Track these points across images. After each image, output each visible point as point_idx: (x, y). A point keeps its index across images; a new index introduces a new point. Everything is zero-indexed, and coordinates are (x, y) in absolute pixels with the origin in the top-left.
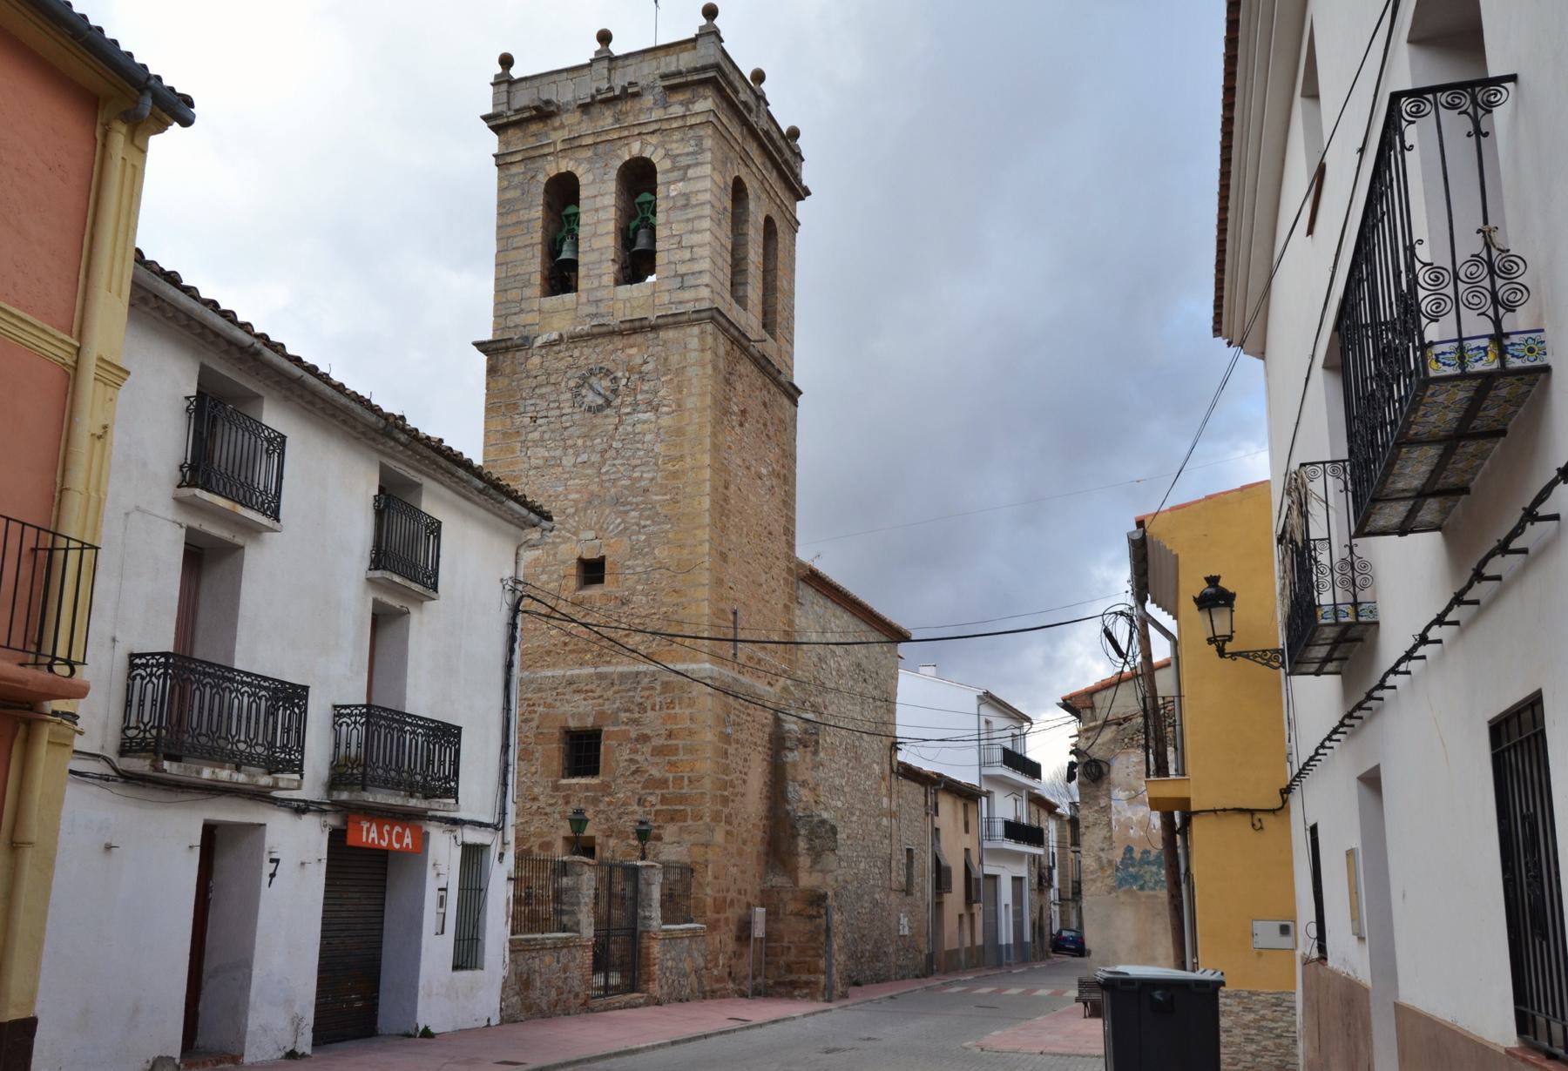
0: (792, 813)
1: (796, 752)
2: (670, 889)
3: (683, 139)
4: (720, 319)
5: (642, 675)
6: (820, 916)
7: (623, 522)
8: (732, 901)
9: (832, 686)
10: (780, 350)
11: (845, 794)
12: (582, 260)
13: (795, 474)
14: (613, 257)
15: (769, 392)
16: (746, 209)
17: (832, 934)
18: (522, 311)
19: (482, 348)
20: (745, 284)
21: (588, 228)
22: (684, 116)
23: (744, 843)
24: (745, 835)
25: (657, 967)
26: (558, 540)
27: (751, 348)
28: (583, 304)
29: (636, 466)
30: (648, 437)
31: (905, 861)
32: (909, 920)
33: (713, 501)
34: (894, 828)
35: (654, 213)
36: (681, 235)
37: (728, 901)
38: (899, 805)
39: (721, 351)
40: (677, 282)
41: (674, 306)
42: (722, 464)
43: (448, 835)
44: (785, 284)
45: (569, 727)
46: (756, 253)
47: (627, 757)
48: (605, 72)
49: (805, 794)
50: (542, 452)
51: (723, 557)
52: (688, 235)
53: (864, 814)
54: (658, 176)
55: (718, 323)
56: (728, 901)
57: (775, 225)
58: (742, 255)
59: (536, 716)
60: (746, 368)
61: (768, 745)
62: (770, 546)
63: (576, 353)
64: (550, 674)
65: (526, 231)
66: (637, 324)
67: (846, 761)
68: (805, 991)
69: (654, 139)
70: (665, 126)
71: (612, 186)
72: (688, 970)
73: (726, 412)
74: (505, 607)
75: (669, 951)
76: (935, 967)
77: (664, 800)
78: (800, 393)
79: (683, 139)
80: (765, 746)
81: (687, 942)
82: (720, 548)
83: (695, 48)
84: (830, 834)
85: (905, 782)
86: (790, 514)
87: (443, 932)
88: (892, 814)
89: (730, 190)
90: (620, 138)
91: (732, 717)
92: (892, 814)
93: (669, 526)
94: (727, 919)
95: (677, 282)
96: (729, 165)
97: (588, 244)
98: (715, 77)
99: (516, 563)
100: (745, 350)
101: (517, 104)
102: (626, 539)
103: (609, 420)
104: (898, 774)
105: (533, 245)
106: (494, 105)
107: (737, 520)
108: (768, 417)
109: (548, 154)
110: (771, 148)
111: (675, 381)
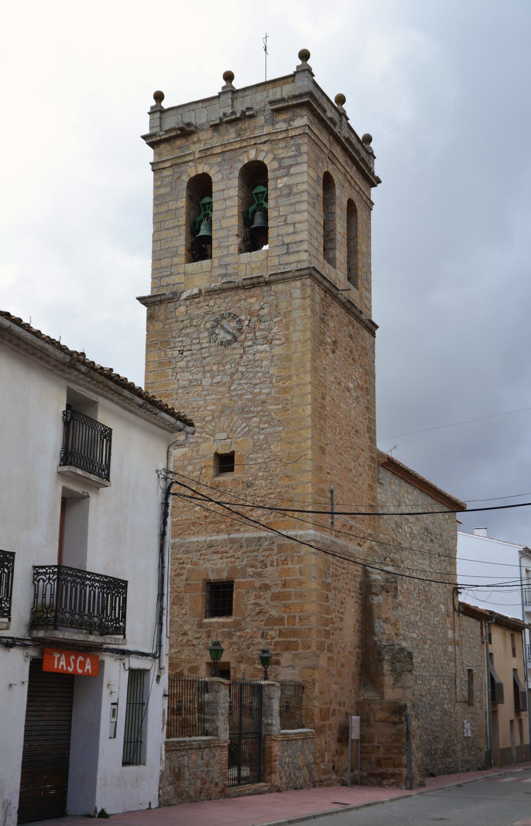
0: (378, 643)
1: (380, 597)
3: (286, 147)
4: (316, 275)
5: (263, 540)
6: (402, 723)
7: (247, 425)
8: (334, 711)
9: (407, 545)
10: (361, 296)
13: (374, 387)
16: (333, 194)
17: (411, 737)
18: (172, 274)
20: (335, 248)
21: (218, 213)
22: (287, 130)
23: (343, 666)
24: (343, 660)
25: (277, 762)
26: (200, 440)
28: (216, 267)
29: (256, 384)
30: (265, 363)
31: (466, 679)
33: (314, 409)
35: (266, 200)
36: (286, 216)
38: (461, 636)
39: (318, 298)
40: (284, 250)
41: (282, 267)
42: (320, 381)
43: (118, 662)
45: (209, 579)
46: (342, 226)
48: (230, 101)
49: (388, 628)
51: (322, 450)
52: (291, 215)
53: (433, 643)
54: (269, 173)
57: (355, 206)
58: (331, 228)
59: (185, 571)
60: (336, 310)
61: (359, 591)
62: (357, 441)
63: (211, 303)
65: (174, 216)
67: (419, 603)
68: (392, 781)
69: (265, 147)
73: (322, 343)
74: (160, 491)
76: (493, 762)
77: (281, 634)
78: (377, 327)
79: (286, 147)
80: (356, 592)
81: (300, 743)
83: (293, 81)
84: (408, 659)
85: (464, 618)
86: (371, 417)
87: (115, 737)
88: (455, 643)
89: (321, 182)
90: (241, 148)
91: (331, 570)
92: (455, 643)
94: (330, 725)
95: (284, 250)
96: (320, 163)
97: (219, 224)
98: (309, 101)
99: (168, 458)
100: (335, 297)
103: (236, 350)
104: (459, 612)
105: (179, 226)
106: (150, 128)
107: (331, 422)
108: (353, 346)
109: (190, 161)
110: (351, 150)
111: (284, 321)
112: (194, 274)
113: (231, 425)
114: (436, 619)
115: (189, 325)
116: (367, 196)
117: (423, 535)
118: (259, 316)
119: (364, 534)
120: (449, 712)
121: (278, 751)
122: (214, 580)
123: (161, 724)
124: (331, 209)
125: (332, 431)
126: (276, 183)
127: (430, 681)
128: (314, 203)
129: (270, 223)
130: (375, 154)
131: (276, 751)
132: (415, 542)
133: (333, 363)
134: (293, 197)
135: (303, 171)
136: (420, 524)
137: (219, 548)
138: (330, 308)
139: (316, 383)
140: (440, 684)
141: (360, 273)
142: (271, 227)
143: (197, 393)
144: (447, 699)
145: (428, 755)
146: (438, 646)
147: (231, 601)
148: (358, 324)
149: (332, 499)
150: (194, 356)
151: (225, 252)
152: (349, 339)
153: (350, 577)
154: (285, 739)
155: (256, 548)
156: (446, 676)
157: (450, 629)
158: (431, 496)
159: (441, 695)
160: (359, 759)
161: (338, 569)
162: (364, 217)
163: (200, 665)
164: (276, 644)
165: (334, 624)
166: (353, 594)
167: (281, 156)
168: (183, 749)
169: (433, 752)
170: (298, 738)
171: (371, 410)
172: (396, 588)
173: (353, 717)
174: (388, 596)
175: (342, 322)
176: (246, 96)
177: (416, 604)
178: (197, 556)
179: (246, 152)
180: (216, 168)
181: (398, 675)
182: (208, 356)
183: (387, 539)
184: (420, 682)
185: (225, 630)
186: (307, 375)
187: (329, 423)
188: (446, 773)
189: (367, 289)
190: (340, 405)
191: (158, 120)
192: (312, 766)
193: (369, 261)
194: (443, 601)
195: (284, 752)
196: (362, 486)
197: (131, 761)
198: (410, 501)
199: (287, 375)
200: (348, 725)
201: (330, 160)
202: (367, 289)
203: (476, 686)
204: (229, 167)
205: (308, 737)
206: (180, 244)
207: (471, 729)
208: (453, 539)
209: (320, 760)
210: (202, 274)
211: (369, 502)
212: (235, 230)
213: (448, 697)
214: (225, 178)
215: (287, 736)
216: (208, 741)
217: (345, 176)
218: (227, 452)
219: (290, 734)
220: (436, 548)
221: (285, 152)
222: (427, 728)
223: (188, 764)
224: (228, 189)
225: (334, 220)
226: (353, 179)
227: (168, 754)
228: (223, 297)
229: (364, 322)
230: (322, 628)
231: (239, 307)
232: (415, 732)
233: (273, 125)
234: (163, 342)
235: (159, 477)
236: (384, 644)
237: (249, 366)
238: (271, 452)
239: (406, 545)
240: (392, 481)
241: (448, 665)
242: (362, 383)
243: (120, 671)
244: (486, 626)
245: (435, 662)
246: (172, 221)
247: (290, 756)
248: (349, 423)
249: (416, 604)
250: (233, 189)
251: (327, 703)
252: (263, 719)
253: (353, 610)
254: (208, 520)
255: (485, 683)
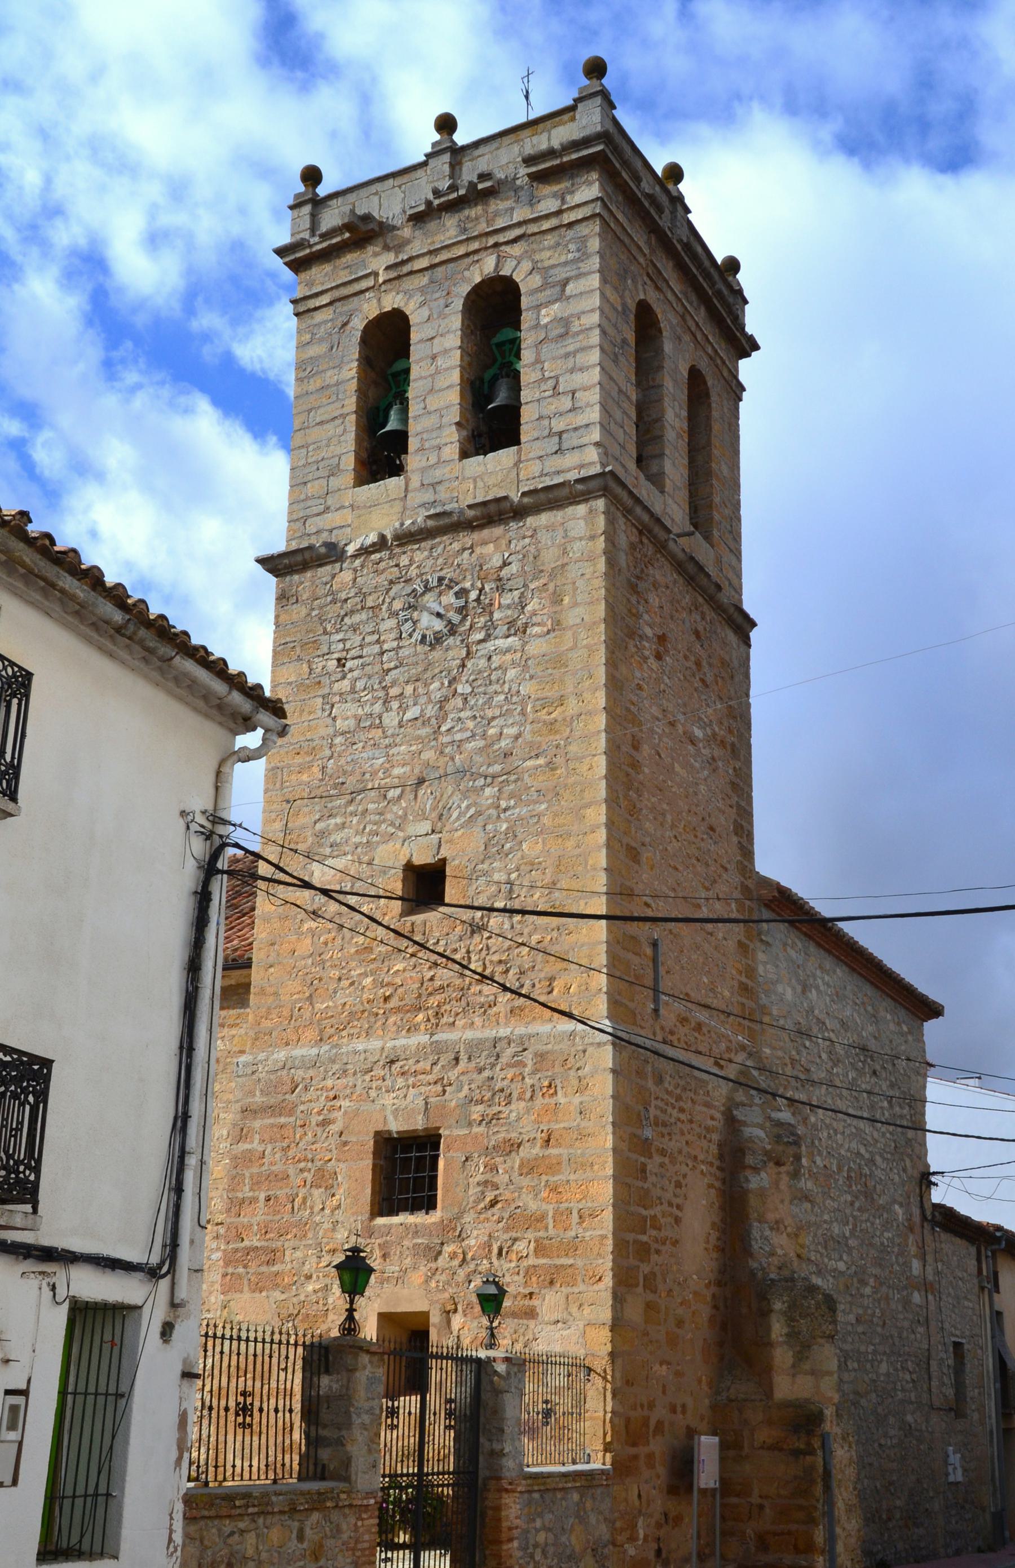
0: (760, 1274)
1: (763, 1175)
2: (546, 1402)
3: (558, 244)
4: (619, 490)
5: (503, 1044)
6: (812, 1452)
8: (660, 1423)
9: (821, 1075)
10: (719, 561)
11: (850, 1250)
12: (413, 428)
13: (749, 746)
14: (458, 419)
15: (703, 619)
16: (659, 351)
17: (834, 1484)
18: (327, 509)
19: (270, 566)
20: (661, 455)
21: (421, 383)
22: (559, 213)
23: (680, 1324)
24: (680, 1311)
25: (516, 1544)
26: (375, 839)
27: (671, 544)
28: (415, 490)
29: (494, 718)
30: (511, 673)
31: (951, 1362)
32: (963, 1457)
33: (611, 766)
34: (932, 1307)
35: (518, 356)
36: (557, 378)
37: (652, 1423)
38: (938, 1273)
39: (623, 541)
40: (553, 444)
41: (547, 478)
42: (628, 710)
43: (33, 1282)
44: (725, 471)
45: (389, 1132)
46: (677, 416)
47: (479, 1178)
48: (447, 168)
49: (782, 1243)
50: (352, 709)
51: (634, 854)
52: (568, 376)
53: (881, 1284)
54: (523, 299)
55: (615, 497)
56: (652, 1423)
57: (705, 383)
58: (654, 416)
59: (338, 1115)
60: (662, 573)
61: (717, 1163)
62: (712, 848)
63: (404, 560)
64: (360, 1047)
65: (334, 398)
66: (493, 508)
67: (849, 1198)
69: (516, 250)
70: (533, 228)
71: (456, 322)
72: (577, 1549)
73: (632, 633)
74: (191, 865)
75: (540, 1515)
76: (1007, 1534)
77: (540, 1249)
78: (753, 624)
79: (558, 244)
80: (711, 1164)
81: (576, 1497)
82: (626, 840)
83: (573, 119)
85: (944, 1236)
86: (743, 804)
87: (15, 1482)
88: (927, 1287)
89: (632, 317)
90: (467, 255)
91: (653, 1112)
92: (927, 1287)
93: (543, 806)
94: (650, 1456)
95: (553, 444)
96: (629, 281)
97: (422, 405)
98: (603, 151)
99: (217, 788)
100: (661, 547)
101: (324, 228)
102: (477, 830)
103: (454, 650)
104: (934, 1223)
105: (344, 416)
106: (292, 235)
107: (653, 800)
108: (704, 655)
109: (367, 290)
110: (694, 270)
111: (551, 587)
112: (370, 507)
113: (440, 805)
114: (886, 1234)
115: (359, 607)
116: (730, 371)
117: (856, 1059)
118: (500, 580)
119: (729, 1044)
120: (917, 1430)
121: (516, 1518)
122: (398, 1132)
123: (175, 1447)
124: (654, 380)
125: (655, 819)
126: (538, 315)
127: (876, 1363)
128: (616, 355)
129: (525, 395)
130: (746, 294)
131: (512, 1516)
132: (840, 1071)
133: (659, 681)
134: (570, 341)
135: (592, 288)
136: (849, 1034)
137: (411, 1062)
138: (650, 568)
139: (618, 712)
140: (896, 1370)
141: (717, 516)
142: (527, 403)
143: (372, 742)
144: (912, 1403)
145: (874, 1522)
146: (891, 1291)
147: (434, 1179)
148: (713, 614)
149: (655, 960)
150: (368, 668)
151: (433, 460)
152: (693, 638)
153: (698, 1130)
154: (536, 1488)
155: (488, 1061)
156: (909, 1354)
157: (915, 1256)
158: (872, 983)
159: (899, 1393)
160: (718, 1533)
161: (669, 1110)
162: (726, 410)
163: (366, 1318)
164: (529, 1271)
165: (660, 1230)
166: (703, 1167)
167: (546, 264)
168: (240, 1515)
169: (884, 1517)
170: (570, 1485)
171: (743, 790)
172: (798, 1158)
173: (703, 1438)
174: (779, 1173)
175: (678, 602)
176: (480, 156)
177: (842, 1199)
178: (364, 1081)
179: (477, 261)
180: (418, 298)
181: (802, 1348)
182: (396, 667)
183: (779, 1058)
184: (852, 1365)
185: (420, 1241)
186: (597, 694)
187: (648, 800)
188: (912, 1560)
189: (731, 551)
190: (673, 768)
191: (307, 218)
192: (606, 1551)
193: (736, 497)
194: (900, 1199)
195: (534, 1520)
196: (724, 942)
197: (86, 1546)
198: (828, 985)
199: (558, 695)
200: (693, 1456)
201: (651, 279)
202: (731, 551)
203: (970, 1378)
204: (444, 293)
205: (595, 1483)
206: (345, 451)
207: (962, 1467)
208: (918, 1073)
209: (626, 1535)
210: (386, 506)
211: (738, 977)
212: (454, 415)
213: (913, 1399)
214: (435, 316)
215: (540, 1481)
216: (319, 1493)
217: (683, 317)
218: (430, 860)
219: (550, 1475)
220: (884, 1088)
221: (557, 255)
222: (870, 1464)
223: (258, 1552)
224: (441, 335)
225: (660, 400)
226: (701, 330)
227: (192, 1528)
228: (429, 546)
229: (724, 611)
230: (630, 1237)
231: (459, 565)
232: (843, 1472)
233: (531, 205)
234: (306, 644)
235: (188, 828)
236: (772, 1276)
237: (479, 682)
238: (523, 858)
239: (819, 1074)
240: (790, 942)
241: (913, 1332)
242: (722, 732)
243: (39, 1305)
244: (987, 1257)
245: (884, 1324)
246: (330, 408)
247: (548, 1530)
248: (693, 808)
249: (842, 1199)
250: (452, 336)
251: (642, 1406)
252: (482, 1440)
253: (704, 1202)
254: (389, 1006)
255: (988, 1372)
